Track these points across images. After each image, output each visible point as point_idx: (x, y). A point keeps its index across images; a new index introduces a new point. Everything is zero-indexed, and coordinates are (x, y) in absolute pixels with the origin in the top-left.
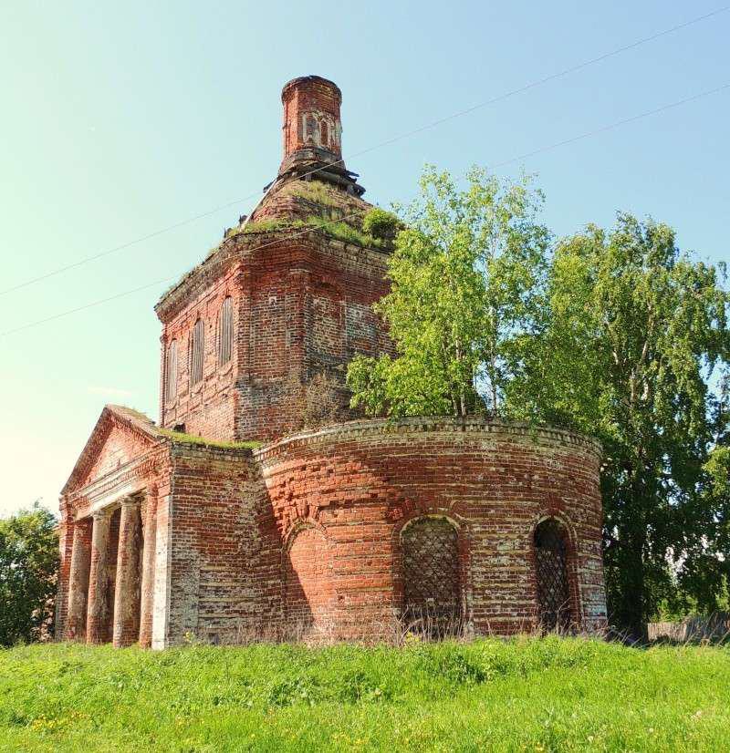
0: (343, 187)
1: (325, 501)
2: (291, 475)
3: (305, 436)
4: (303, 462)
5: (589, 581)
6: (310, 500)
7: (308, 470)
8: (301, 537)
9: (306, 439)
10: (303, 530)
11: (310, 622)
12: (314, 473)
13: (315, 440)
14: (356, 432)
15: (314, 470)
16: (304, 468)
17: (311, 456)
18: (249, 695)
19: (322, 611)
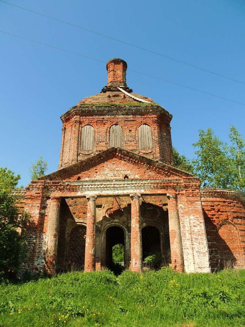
0: (119, 91)
1: (235, 215)
2: (219, 203)
3: (227, 191)
4: (224, 200)
5: (111, 282)
6: (229, 214)
7: (226, 203)
8: (223, 227)
9: (227, 192)
10: (225, 224)
11: (234, 260)
12: (229, 205)
13: (222, 193)
14: (93, 186)
15: (228, 204)
16: (224, 202)
17: (227, 198)
18: (172, 297)
19: (238, 255)
